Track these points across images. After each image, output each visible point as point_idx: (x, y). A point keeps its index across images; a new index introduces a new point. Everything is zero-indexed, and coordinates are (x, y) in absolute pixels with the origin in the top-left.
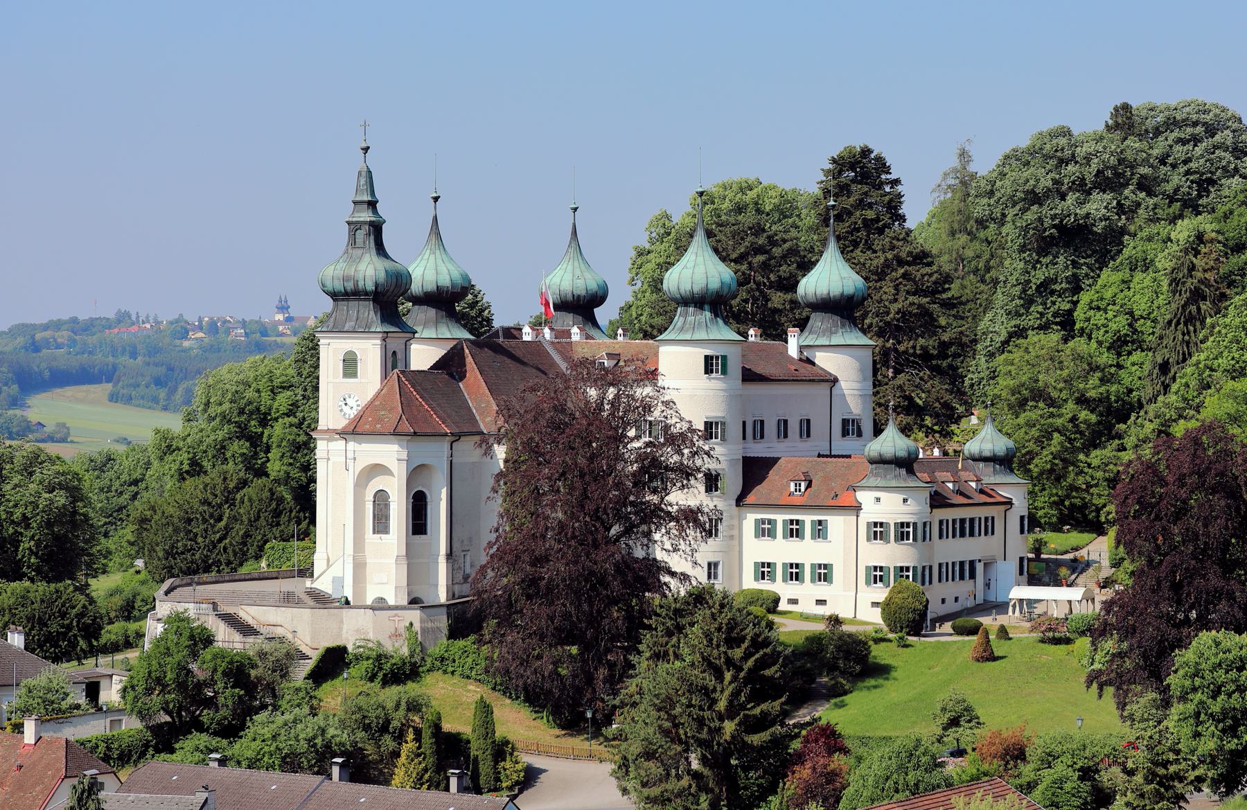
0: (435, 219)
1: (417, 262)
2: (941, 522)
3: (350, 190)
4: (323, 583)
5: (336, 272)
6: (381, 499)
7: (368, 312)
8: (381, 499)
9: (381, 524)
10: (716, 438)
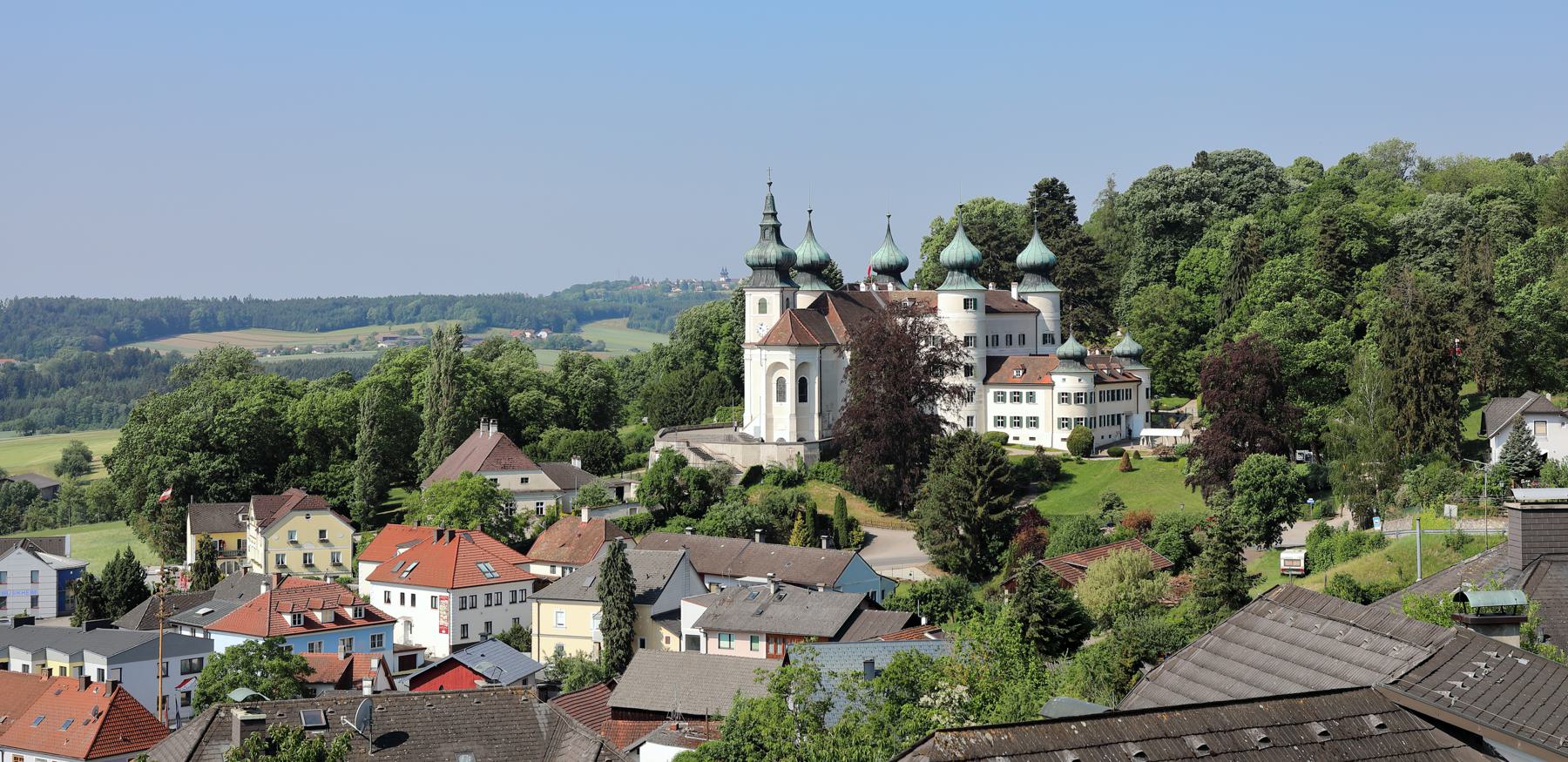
0: (810, 223)
2: (1100, 392)
3: (761, 206)
4: (749, 430)
6: (781, 382)
8: (781, 382)
9: (781, 396)
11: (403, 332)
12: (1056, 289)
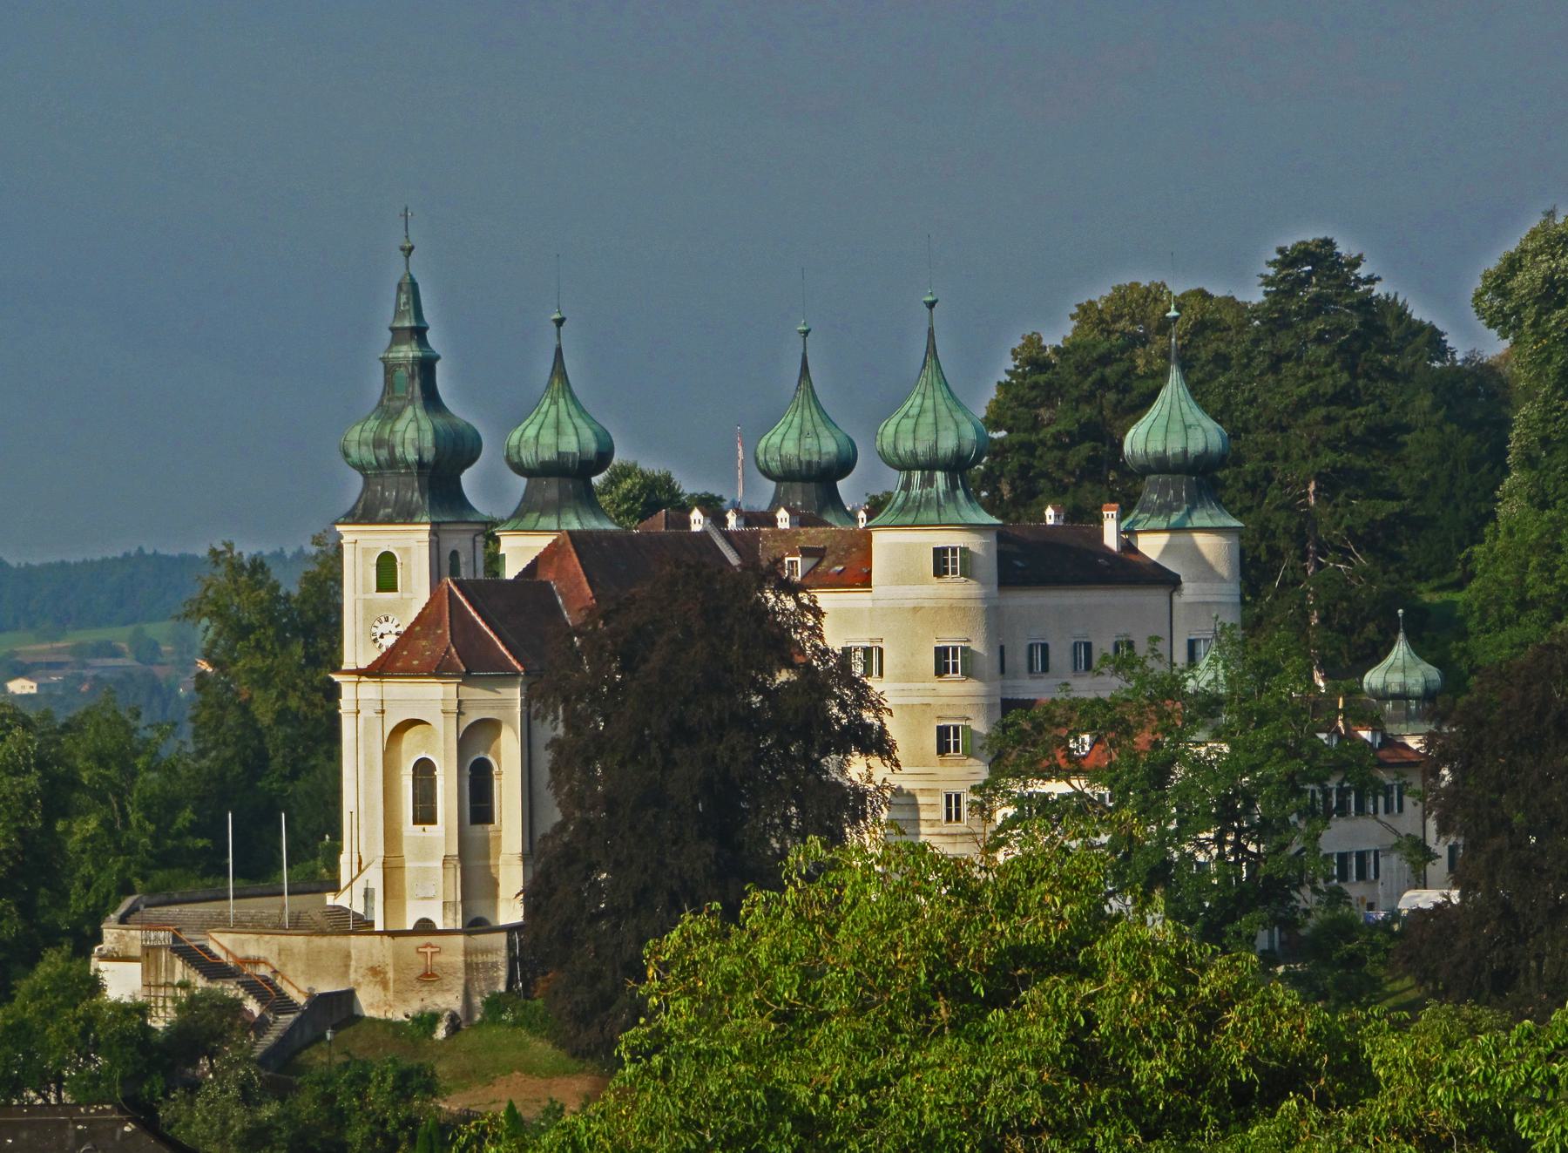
1: (532, 417)
2: (958, 818)
3: (387, 312)
4: (348, 899)
5: (365, 435)
6: (424, 769)
8: (424, 769)
9: (425, 815)
10: (955, 671)
11: (79, 651)
12: (1235, 523)
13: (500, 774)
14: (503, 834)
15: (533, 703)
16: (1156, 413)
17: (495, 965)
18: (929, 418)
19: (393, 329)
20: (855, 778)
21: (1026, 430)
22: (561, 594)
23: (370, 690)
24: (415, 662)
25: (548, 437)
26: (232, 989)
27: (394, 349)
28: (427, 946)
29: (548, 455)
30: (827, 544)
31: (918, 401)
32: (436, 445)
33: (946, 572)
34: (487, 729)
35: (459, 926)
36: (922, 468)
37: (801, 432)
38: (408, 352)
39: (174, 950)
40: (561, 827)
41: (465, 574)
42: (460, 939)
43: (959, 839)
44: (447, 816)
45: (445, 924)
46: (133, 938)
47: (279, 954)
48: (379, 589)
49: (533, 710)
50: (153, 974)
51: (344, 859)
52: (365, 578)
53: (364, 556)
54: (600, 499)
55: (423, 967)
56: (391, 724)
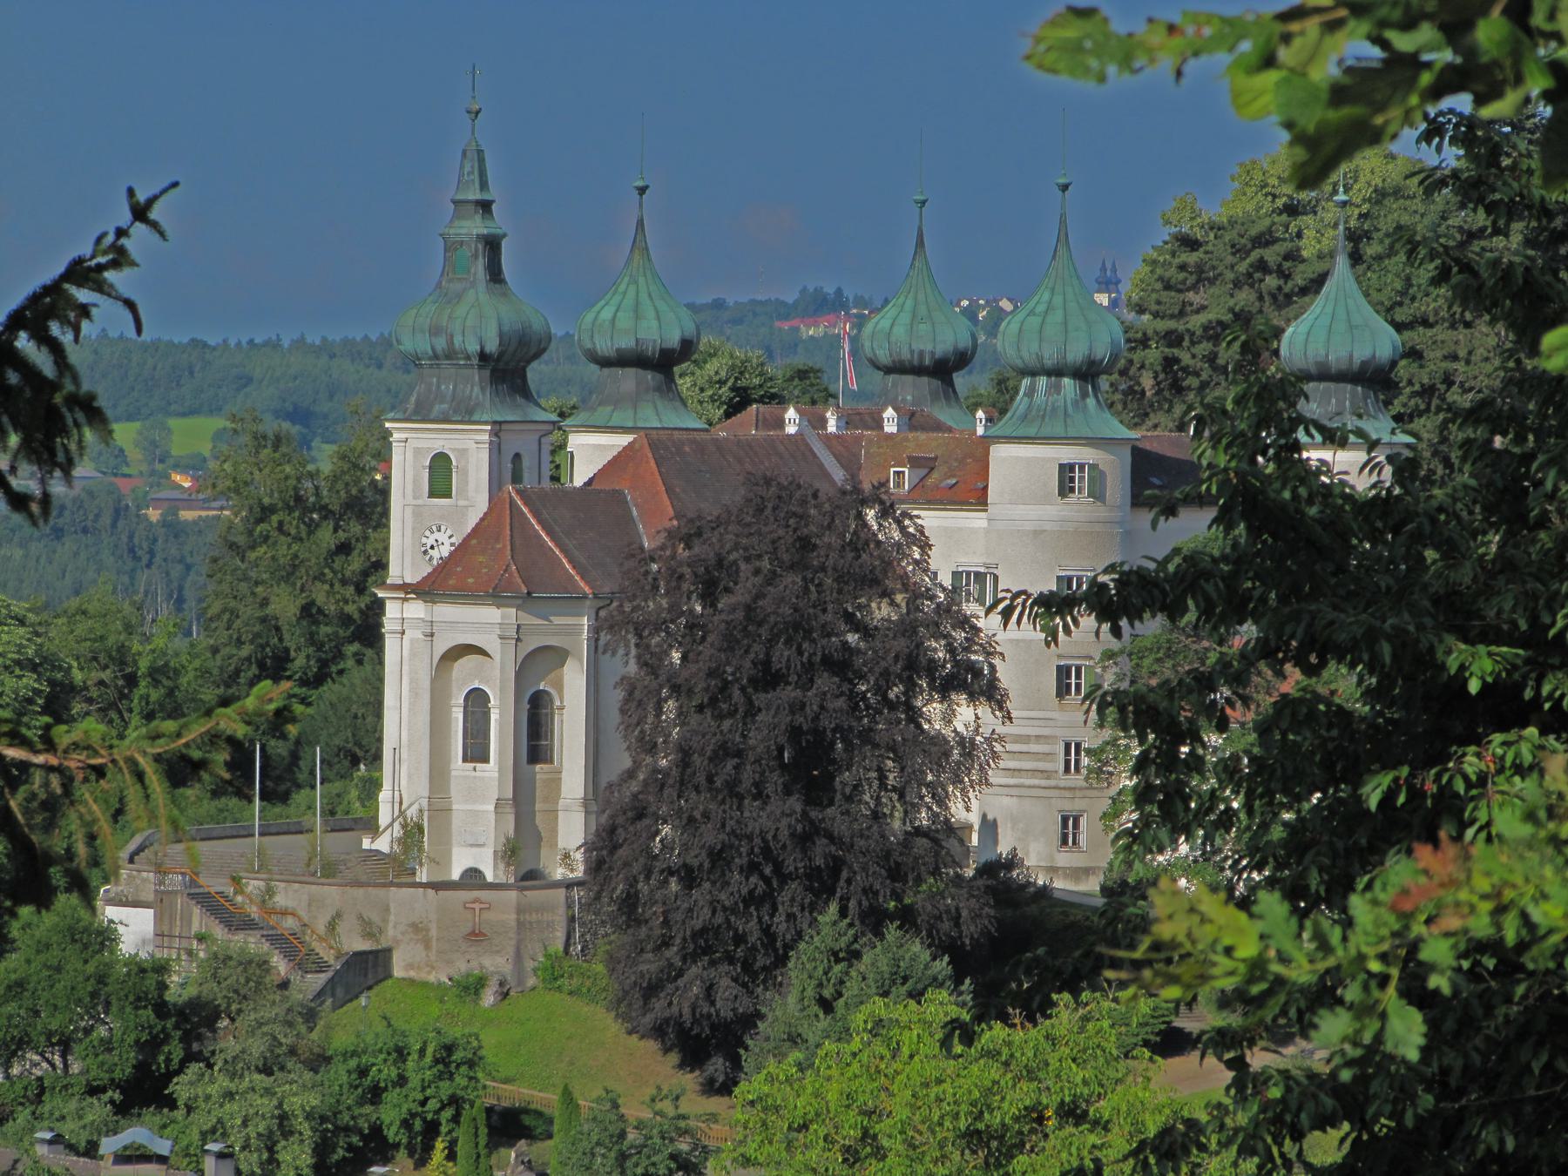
6: (477, 699)
7: (474, 385)
8: (477, 699)
9: (476, 752)
13: (562, 708)
14: (564, 774)
15: (602, 634)
16: (1318, 310)
17: (550, 925)
18: (1058, 316)
19: (455, 202)
20: (961, 728)
21: (1172, 316)
22: (637, 506)
23: (416, 609)
24: (471, 580)
25: (625, 321)
26: (253, 943)
27: (456, 223)
28: (476, 901)
29: (626, 343)
30: (939, 453)
31: (1046, 296)
32: (501, 335)
33: (1072, 490)
34: (549, 657)
35: (512, 880)
36: (1049, 373)
37: (914, 316)
38: (475, 226)
39: (192, 896)
40: (630, 774)
41: (529, 481)
42: (513, 894)
43: (1078, 794)
44: (501, 753)
45: (495, 876)
46: (145, 880)
47: (309, 905)
48: (432, 495)
49: (602, 643)
50: (166, 922)
51: (384, 796)
52: (416, 481)
53: (415, 457)
54: (680, 382)
55: (470, 925)
56: (442, 646)
